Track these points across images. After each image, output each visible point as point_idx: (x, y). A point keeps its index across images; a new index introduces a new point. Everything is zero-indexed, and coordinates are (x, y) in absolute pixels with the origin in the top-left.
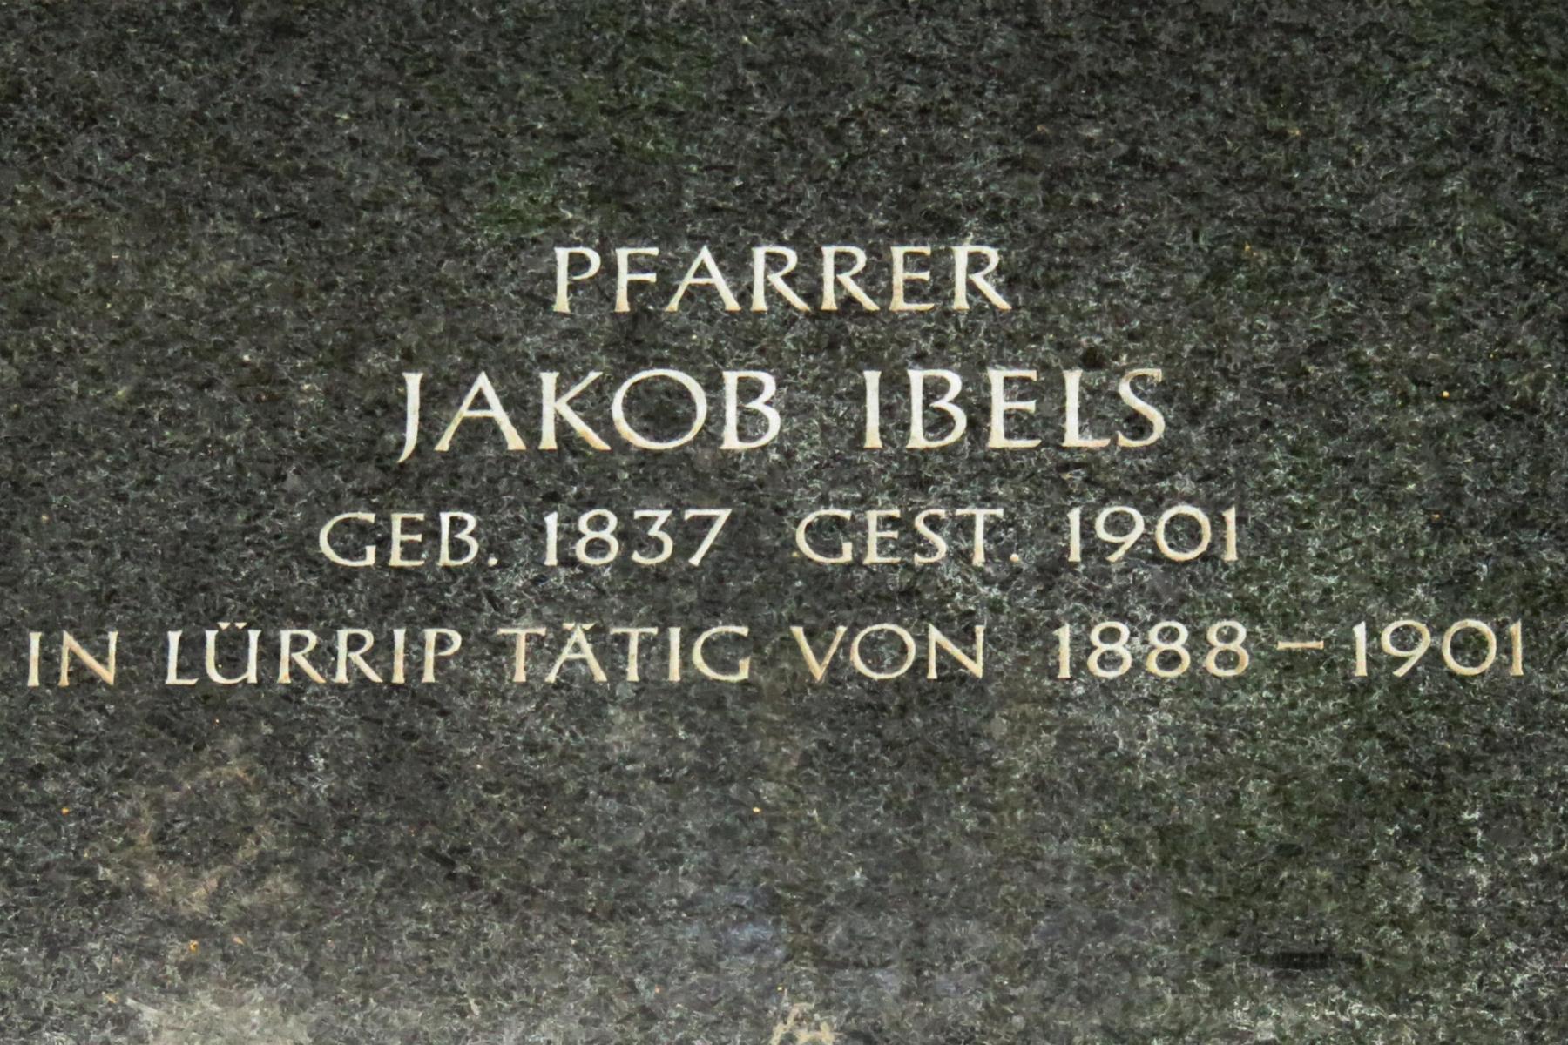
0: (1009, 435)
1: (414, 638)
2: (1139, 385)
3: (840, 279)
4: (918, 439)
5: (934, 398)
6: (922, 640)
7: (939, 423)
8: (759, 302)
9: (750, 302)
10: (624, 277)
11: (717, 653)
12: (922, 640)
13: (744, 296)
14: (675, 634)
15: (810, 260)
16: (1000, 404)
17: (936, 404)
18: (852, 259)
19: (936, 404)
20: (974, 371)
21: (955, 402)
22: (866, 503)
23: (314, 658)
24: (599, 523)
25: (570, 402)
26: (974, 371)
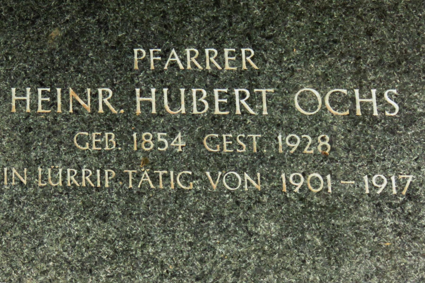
0: (42, 109)
1: (102, 174)
2: (390, 95)
3: (211, 60)
4: (195, 111)
5: (199, 98)
6: (242, 177)
7: (201, 107)
8: (189, 67)
9: (186, 67)
10: (152, 58)
11: (186, 179)
12: (242, 177)
13: (185, 67)
14: (172, 173)
15: (202, 53)
16: (217, 101)
17: (199, 100)
18: (214, 53)
19: (199, 100)
20: (210, 89)
21: (205, 99)
22: (92, 131)
23: (91, 178)
24: (147, 137)
25: (245, 101)
26: (210, 89)
